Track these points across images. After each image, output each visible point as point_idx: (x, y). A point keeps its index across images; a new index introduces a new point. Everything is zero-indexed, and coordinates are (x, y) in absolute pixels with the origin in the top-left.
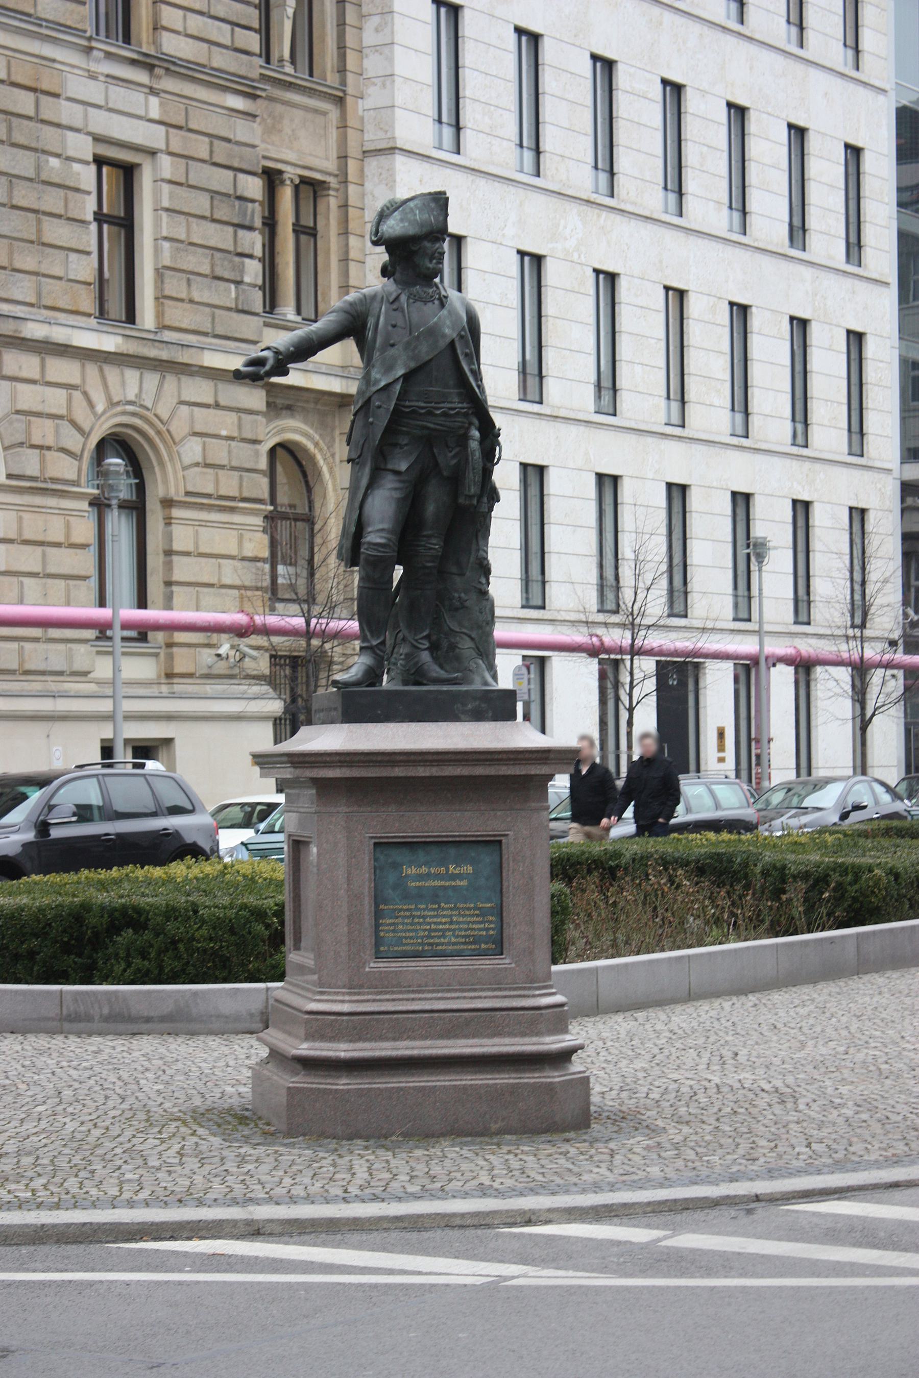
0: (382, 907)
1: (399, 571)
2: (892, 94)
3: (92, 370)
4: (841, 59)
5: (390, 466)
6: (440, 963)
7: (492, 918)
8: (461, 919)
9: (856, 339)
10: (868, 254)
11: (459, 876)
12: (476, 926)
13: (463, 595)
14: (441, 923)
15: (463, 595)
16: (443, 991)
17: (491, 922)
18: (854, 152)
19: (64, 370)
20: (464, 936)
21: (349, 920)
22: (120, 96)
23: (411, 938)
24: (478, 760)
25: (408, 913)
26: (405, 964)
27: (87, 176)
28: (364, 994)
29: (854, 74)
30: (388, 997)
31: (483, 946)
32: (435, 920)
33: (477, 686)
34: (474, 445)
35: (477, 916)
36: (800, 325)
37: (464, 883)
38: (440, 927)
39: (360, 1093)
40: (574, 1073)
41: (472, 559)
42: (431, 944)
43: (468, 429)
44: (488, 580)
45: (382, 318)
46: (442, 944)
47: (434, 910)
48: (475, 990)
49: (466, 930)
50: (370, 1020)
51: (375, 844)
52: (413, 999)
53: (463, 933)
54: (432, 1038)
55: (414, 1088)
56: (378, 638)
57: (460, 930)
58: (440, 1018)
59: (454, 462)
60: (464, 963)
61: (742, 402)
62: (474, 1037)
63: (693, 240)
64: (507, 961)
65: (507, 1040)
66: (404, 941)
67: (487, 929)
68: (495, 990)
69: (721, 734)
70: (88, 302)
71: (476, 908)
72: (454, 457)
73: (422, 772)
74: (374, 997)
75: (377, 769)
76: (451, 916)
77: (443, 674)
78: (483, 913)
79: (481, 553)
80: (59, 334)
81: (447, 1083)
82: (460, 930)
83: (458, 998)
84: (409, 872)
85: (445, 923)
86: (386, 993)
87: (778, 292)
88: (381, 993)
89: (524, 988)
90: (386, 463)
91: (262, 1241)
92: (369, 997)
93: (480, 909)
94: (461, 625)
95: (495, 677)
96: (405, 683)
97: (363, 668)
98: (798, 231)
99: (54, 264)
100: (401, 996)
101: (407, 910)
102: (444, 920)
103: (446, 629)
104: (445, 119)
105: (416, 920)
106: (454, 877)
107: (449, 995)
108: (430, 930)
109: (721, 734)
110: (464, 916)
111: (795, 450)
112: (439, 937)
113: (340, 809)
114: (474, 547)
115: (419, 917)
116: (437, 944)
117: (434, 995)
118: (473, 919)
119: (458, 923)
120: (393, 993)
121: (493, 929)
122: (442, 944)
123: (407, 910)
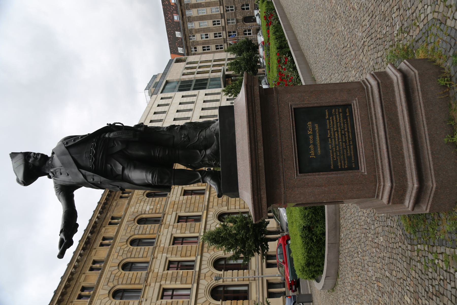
0: (332, 167)
1: (179, 166)
3: (211, 195)
5: (121, 173)
6: (359, 136)
7: (333, 111)
8: (335, 126)
9: (206, 95)
10: (195, 94)
11: (314, 128)
12: (338, 119)
13: (183, 136)
14: (338, 136)
15: (183, 136)
16: (374, 133)
17: (335, 111)
18: (183, 97)
19: (211, 199)
20: (344, 124)
21: (341, 185)
22: (175, 193)
23: (347, 152)
24: (253, 121)
25: (335, 154)
26: (361, 154)
27: (186, 197)
28: (379, 175)
30: (379, 162)
31: (348, 114)
32: (337, 140)
35: (333, 118)
36: (204, 102)
37: (316, 125)
38: (340, 137)
39: (437, 175)
40: (408, 66)
42: (349, 141)
43: (106, 138)
44: (177, 126)
45: (64, 179)
46: (349, 135)
47: (331, 140)
48: (371, 117)
49: (340, 124)
50: (394, 171)
51: (300, 173)
52: (380, 149)
53: (342, 125)
55: (431, 145)
56: (198, 175)
57: (340, 126)
59: (120, 143)
60: (358, 123)
62: (398, 116)
64: (355, 102)
65: (398, 99)
66: (349, 155)
67: (339, 113)
70: (202, 196)
71: (329, 119)
72: (118, 144)
73: (261, 151)
74: (380, 169)
76: (334, 132)
78: (330, 115)
79: (165, 130)
80: (207, 200)
81: (426, 128)
83: (377, 125)
84: (313, 154)
85: (338, 134)
87: (200, 104)
88: (378, 166)
89: (368, 92)
90: (119, 175)
92: (381, 172)
93: (329, 117)
97: (212, 182)
98: (193, 102)
99: (197, 201)
100: (379, 155)
102: (336, 135)
105: (338, 149)
106: (314, 131)
108: (342, 142)
110: (333, 125)
112: (345, 137)
113: (283, 192)
114: (162, 133)
115: (336, 148)
116: (349, 138)
118: (335, 120)
119: (337, 127)
120: (377, 159)
121: (339, 110)
122: (349, 135)
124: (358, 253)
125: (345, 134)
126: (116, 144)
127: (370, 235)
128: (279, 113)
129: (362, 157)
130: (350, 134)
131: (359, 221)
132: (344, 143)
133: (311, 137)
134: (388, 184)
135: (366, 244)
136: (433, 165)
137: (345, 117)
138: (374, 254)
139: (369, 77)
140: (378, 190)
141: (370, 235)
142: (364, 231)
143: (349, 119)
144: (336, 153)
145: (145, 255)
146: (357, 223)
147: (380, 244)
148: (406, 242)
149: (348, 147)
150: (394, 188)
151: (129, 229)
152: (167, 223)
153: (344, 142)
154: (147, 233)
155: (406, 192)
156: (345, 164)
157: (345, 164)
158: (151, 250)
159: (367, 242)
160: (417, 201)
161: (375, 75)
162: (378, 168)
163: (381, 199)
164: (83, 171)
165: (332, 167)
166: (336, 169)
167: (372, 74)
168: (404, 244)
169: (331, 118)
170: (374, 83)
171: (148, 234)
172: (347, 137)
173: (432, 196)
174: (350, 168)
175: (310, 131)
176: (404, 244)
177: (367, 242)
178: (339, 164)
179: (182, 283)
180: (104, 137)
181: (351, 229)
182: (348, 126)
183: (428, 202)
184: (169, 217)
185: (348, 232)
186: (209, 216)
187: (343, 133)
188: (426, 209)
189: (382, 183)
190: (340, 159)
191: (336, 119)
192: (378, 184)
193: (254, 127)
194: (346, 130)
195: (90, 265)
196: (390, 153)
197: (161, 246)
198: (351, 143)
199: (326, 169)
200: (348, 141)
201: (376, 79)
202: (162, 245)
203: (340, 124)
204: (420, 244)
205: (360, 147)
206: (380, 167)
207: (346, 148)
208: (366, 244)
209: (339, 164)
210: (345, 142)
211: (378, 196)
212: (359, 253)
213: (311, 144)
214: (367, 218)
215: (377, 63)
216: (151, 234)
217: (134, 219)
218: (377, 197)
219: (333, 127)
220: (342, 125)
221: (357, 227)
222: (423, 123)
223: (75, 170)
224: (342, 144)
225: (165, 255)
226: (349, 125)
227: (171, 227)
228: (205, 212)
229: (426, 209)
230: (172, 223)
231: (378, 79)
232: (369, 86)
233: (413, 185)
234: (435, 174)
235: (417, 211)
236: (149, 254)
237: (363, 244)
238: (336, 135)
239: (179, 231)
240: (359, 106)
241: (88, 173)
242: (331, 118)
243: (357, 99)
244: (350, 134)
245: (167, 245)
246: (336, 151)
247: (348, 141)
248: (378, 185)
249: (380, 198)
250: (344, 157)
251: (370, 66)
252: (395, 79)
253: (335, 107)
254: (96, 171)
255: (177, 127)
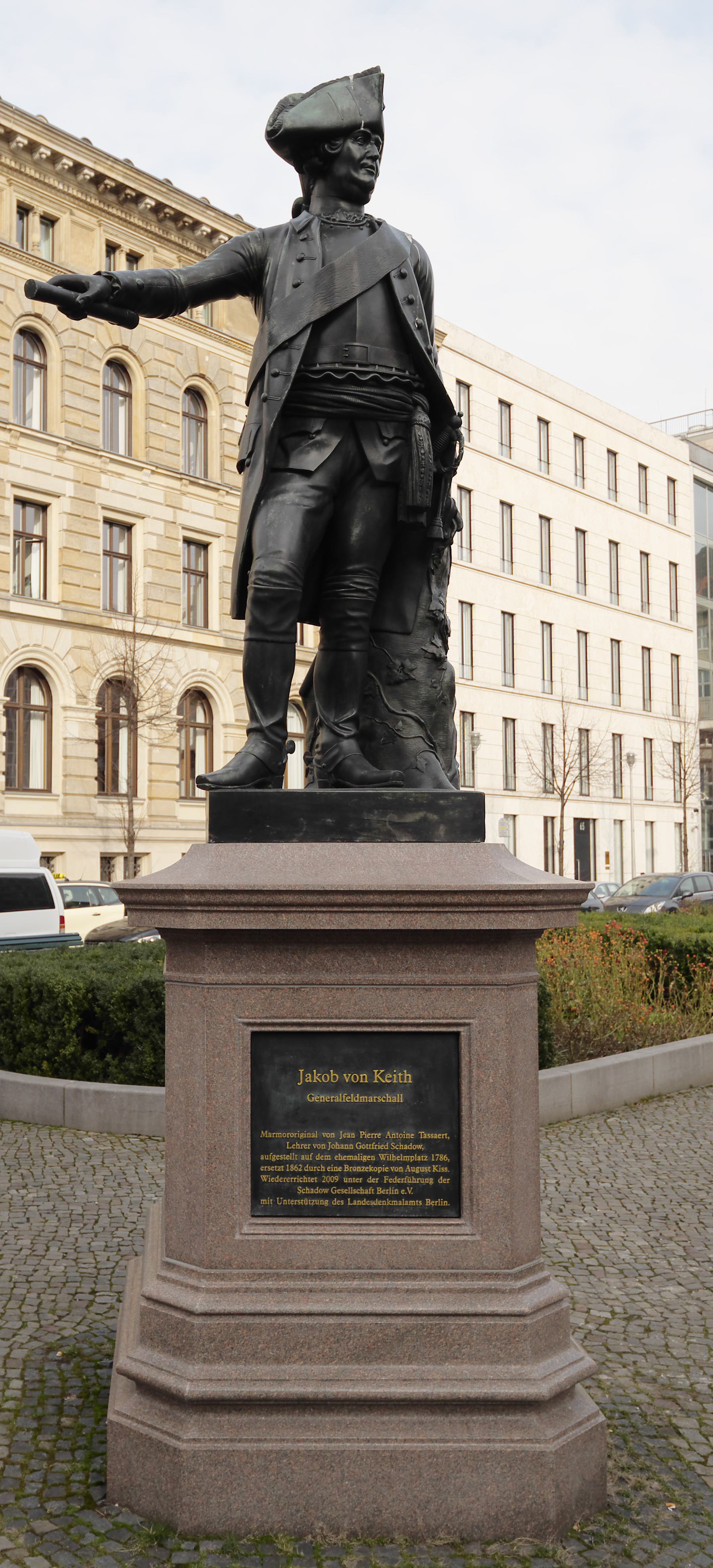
0: (265, 1134)
2: (693, 538)
4: (667, 520)
5: (293, 465)
11: (392, 1088)
14: (360, 1163)
17: (443, 1164)
20: (400, 1186)
29: (673, 527)
30: (270, 1284)
31: (429, 1202)
32: (350, 1158)
33: (428, 789)
34: (421, 434)
35: (419, 1152)
37: (399, 1098)
38: (358, 1169)
41: (421, 613)
42: (344, 1197)
43: (411, 413)
48: (415, 1277)
49: (399, 1175)
50: (237, 1327)
51: (253, 1034)
53: (397, 1180)
54: (340, 1361)
57: (391, 1174)
58: (354, 1327)
61: (617, 688)
63: (592, 607)
65: (466, 1369)
66: (300, 1190)
67: (436, 1176)
68: (447, 1277)
69: (607, 855)
71: (417, 1141)
75: (252, 917)
76: (375, 1152)
77: (373, 772)
78: (432, 1147)
82: (391, 1174)
84: (309, 1080)
85: (366, 1164)
86: (267, 1277)
90: (287, 457)
91: (492, 886)
92: (240, 1283)
93: (424, 1141)
94: (405, 706)
95: (454, 779)
96: (323, 785)
98: (646, 603)
101: (305, 1141)
102: (365, 1158)
103: (384, 712)
104: (464, 545)
105: (319, 1157)
106: (380, 1088)
107: (370, 1284)
108: (342, 1174)
109: (607, 855)
110: (396, 1152)
111: (644, 713)
112: (356, 1186)
114: (425, 595)
115: (323, 1152)
117: (347, 1283)
119: (390, 1164)
121: (445, 1175)
123: (305, 1141)
124: (24, 1187)
125: (365, 1185)
126: (391, 446)
127: (74, 1231)
128: (446, 984)
129: (291, 1230)
130: (365, 1202)
131: (127, 1200)
132: (336, 1178)
133: (363, 1078)
134: (198, 1303)
135: (48, 1217)
136: (246, 1452)
137: (420, 1192)
138: (12, 1240)
139: (555, 1288)
140: (187, 1270)
141: (74, 1231)
142: (90, 1217)
143: (412, 1202)
144: (307, 1152)
145: (72, 416)
146: (120, 1193)
147: (44, 1262)
148: (35, 1344)
149: (326, 1191)
150: (188, 1319)
151: (170, 357)
152: (186, 502)
153: (341, 1180)
154: (152, 423)
155: (174, 1355)
156: (274, 1174)
157: (274, 1174)
158: (87, 438)
159: (53, 1221)
160: (146, 1388)
161: (556, 1309)
162: (252, 1278)
163: (159, 1277)
164: (303, 341)
165: (265, 1134)
166: (258, 1147)
167: (560, 1301)
168: (33, 1338)
169: (420, 1147)
170: (526, 1303)
171: (147, 427)
172: (355, 1192)
173: (156, 1435)
174: (258, 1190)
175: (383, 1075)
176: (33, 1338)
177: (53, 1221)
178: (274, 1158)
179: (148, 551)
180: (416, 404)
181: (106, 1172)
182: (392, 1197)
183: (138, 1421)
184: (208, 508)
185: (96, 1161)
186: (204, 654)
187: (371, 1180)
188: (118, 1413)
189: (204, 1284)
190: (290, 1162)
191: (415, 1164)
192: (205, 1271)
193: (400, 905)
194: (380, 1191)
195: (41, 208)
196: (295, 1320)
197: (103, 477)
198: (336, 1202)
199: (261, 1113)
200: (344, 1191)
201: (538, 1310)
202: (104, 480)
203: (399, 1175)
204: (24, 1386)
205: (321, 1230)
206: (254, 1285)
207: (322, 1185)
208: (48, 1217)
209: (274, 1158)
210: (340, 1184)
211: (169, 1266)
212: (23, 1192)
213: (341, 1076)
214: (131, 1227)
215: (648, 1330)
216: (147, 440)
217: (202, 376)
218: (168, 1264)
219: (390, 1151)
220: (397, 1180)
221: (108, 1192)
222: (379, 1441)
223: (315, 311)
224: (333, 1174)
225: (69, 489)
226: (395, 1202)
227: (168, 514)
228: (220, 643)
229: (118, 1413)
230: (184, 518)
231: (540, 1316)
232: (519, 1284)
233: (192, 1379)
234: (218, 1453)
235: (119, 1387)
236: (77, 434)
237: (49, 1205)
238: (365, 1158)
239: (153, 543)
240: (454, 1244)
241: (297, 356)
242: (420, 1147)
243: (478, 1237)
244: (365, 1202)
245: (102, 497)
246: (316, 1151)
247: (344, 1191)
248: (199, 1269)
249: (164, 1273)
250: (294, 1174)
251: (644, 1305)
252: (536, 1370)
253: (456, 1165)
254: (303, 382)
255: (439, 643)
